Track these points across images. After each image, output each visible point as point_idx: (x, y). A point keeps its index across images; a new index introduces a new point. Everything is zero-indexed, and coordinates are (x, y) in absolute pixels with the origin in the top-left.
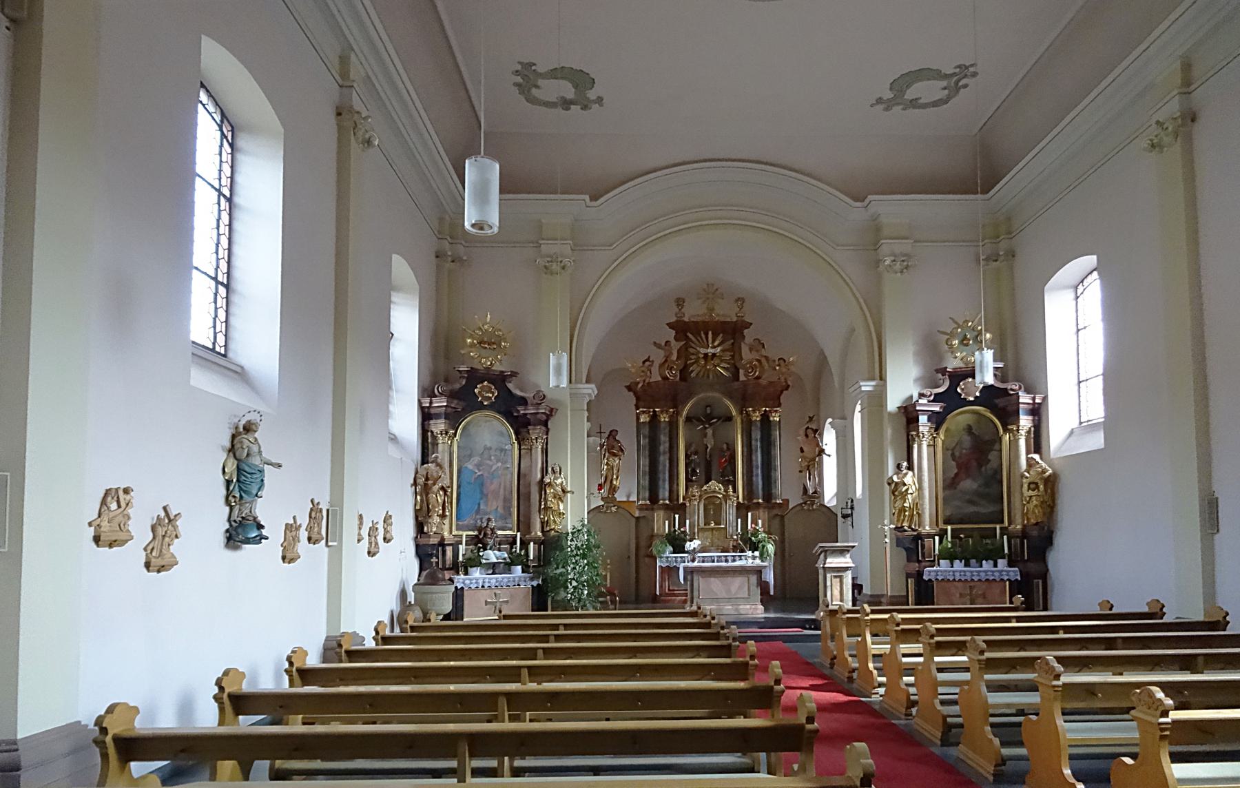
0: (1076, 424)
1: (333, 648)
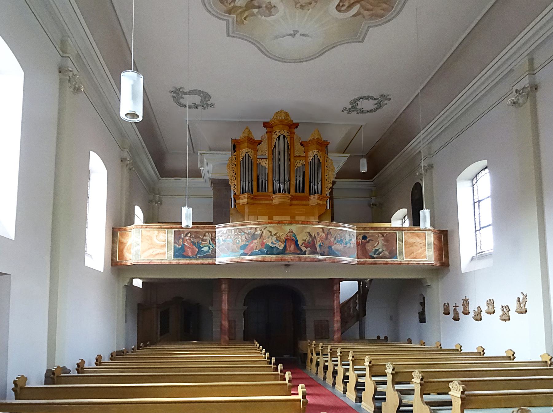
0: (474, 254)
1: (52, 376)
